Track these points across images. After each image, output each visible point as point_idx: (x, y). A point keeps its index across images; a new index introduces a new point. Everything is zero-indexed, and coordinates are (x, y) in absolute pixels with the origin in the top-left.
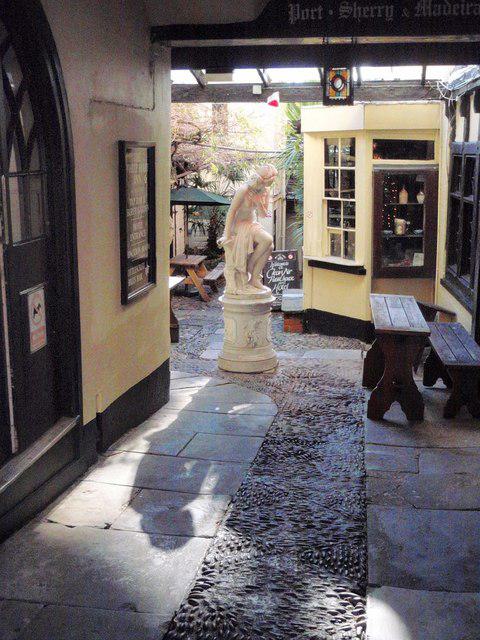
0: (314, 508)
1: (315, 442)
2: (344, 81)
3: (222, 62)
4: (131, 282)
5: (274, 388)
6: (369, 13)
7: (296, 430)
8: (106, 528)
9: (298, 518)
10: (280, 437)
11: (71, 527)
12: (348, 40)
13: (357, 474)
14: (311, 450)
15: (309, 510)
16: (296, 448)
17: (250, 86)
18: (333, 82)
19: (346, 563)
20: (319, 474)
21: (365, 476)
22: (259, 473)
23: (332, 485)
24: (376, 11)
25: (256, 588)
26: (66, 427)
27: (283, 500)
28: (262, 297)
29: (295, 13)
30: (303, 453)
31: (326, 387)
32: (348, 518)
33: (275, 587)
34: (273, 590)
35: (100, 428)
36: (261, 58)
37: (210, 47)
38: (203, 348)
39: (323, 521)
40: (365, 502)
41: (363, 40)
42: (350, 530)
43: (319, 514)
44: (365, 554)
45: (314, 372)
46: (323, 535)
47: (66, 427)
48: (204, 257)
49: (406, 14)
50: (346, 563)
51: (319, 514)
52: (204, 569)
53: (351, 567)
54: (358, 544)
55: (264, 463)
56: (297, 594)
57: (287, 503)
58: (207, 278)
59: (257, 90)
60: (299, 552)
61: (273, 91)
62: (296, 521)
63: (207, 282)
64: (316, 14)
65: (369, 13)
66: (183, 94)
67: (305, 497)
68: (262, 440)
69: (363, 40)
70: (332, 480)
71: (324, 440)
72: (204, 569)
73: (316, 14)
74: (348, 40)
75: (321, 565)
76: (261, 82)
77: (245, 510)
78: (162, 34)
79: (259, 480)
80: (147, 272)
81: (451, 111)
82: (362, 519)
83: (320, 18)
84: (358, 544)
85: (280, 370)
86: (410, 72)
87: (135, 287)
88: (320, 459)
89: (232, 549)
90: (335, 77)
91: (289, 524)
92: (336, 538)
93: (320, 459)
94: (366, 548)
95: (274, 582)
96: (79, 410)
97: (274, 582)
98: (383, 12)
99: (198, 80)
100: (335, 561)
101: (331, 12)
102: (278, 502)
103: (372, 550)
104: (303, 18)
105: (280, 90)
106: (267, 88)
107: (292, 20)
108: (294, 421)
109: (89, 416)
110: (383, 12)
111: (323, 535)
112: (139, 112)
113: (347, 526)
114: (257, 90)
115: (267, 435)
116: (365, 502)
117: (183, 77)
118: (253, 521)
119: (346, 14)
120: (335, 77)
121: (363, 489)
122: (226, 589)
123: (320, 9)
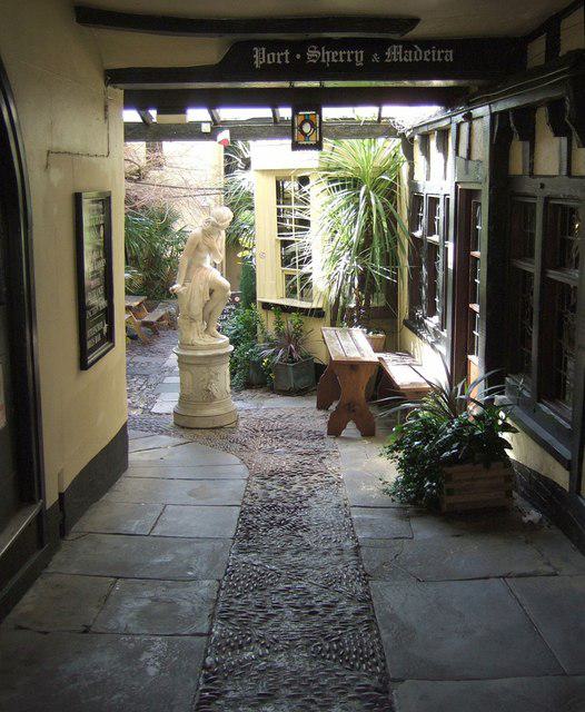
0: (313, 590)
1: (296, 508)
2: (313, 125)
3: (175, 103)
4: (89, 345)
5: (239, 447)
6: (337, 58)
7: (272, 495)
8: (85, 632)
9: (298, 604)
10: (258, 506)
11: (46, 633)
12: (316, 84)
13: (349, 544)
14: (294, 518)
15: (308, 593)
16: (279, 516)
17: (198, 124)
18: (301, 127)
19: (362, 655)
20: (309, 548)
21: (358, 547)
22: (243, 550)
23: (323, 561)
24: (345, 57)
25: (269, 695)
26: (33, 512)
27: (278, 582)
28: (220, 346)
29: (260, 58)
30: (287, 522)
31: (296, 442)
32: (351, 598)
33: (290, 693)
34: (289, 697)
35: (62, 509)
36: (212, 100)
37: (161, 95)
38: (152, 402)
39: (324, 606)
40: (366, 577)
41: (329, 84)
42: (357, 614)
43: (319, 598)
44: (378, 642)
45: (278, 424)
46: (330, 622)
47: (33, 512)
48: (143, 298)
49: (376, 58)
50: (362, 655)
51: (319, 598)
52: (206, 676)
53: (368, 659)
54: (369, 630)
55: (248, 538)
56: (316, 699)
57: (282, 586)
58: (146, 319)
59: (206, 128)
60: (308, 646)
61: (223, 129)
62: (297, 608)
63: (145, 324)
64: (283, 58)
65: (337, 58)
66: (132, 132)
67: (300, 577)
68: (238, 510)
69: (329, 84)
70: (325, 554)
71: (305, 505)
72: (206, 676)
73: (283, 58)
74: (316, 84)
75: (335, 660)
76: (210, 119)
77: (238, 597)
78: (113, 77)
79: (245, 559)
80: (105, 330)
81: (408, 146)
82: (367, 600)
83: (287, 62)
84: (369, 630)
85: (241, 423)
86: (366, 113)
87: (93, 350)
88: (306, 529)
89: (233, 649)
90: (303, 123)
91: (289, 613)
92: (345, 625)
93: (306, 529)
94: (378, 635)
95: (287, 686)
96: (41, 495)
97: (287, 686)
98: (353, 56)
99: (142, 118)
100: (349, 653)
101: (298, 56)
102: (272, 585)
103: (385, 636)
104: (269, 62)
105: (231, 129)
106: (217, 126)
107: (257, 64)
108: (268, 484)
109: (51, 497)
110: (353, 56)
111: (330, 622)
112: (94, 159)
113: (352, 609)
114: (206, 128)
115: (243, 503)
116: (366, 577)
117: (132, 116)
118: (249, 611)
119: (314, 58)
120: (303, 123)
121: (360, 561)
122: (234, 699)
123: (287, 53)
